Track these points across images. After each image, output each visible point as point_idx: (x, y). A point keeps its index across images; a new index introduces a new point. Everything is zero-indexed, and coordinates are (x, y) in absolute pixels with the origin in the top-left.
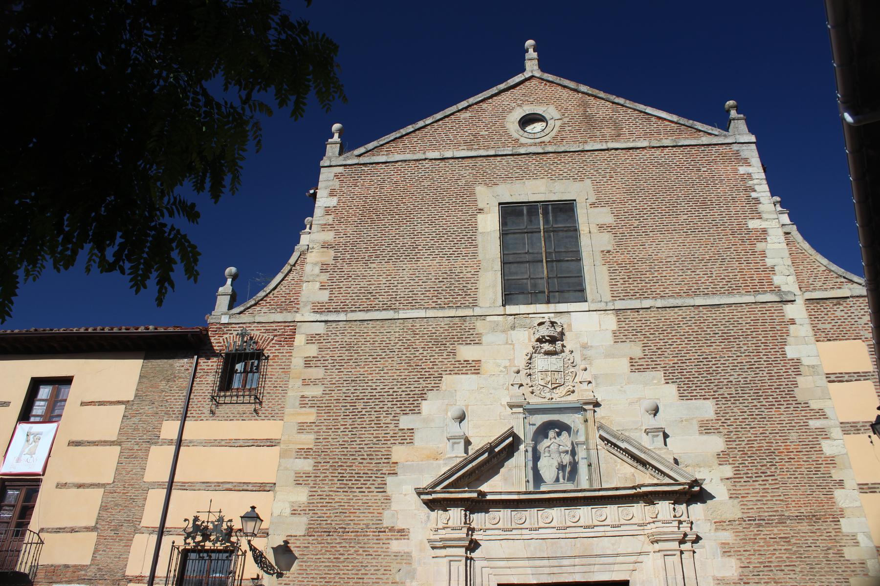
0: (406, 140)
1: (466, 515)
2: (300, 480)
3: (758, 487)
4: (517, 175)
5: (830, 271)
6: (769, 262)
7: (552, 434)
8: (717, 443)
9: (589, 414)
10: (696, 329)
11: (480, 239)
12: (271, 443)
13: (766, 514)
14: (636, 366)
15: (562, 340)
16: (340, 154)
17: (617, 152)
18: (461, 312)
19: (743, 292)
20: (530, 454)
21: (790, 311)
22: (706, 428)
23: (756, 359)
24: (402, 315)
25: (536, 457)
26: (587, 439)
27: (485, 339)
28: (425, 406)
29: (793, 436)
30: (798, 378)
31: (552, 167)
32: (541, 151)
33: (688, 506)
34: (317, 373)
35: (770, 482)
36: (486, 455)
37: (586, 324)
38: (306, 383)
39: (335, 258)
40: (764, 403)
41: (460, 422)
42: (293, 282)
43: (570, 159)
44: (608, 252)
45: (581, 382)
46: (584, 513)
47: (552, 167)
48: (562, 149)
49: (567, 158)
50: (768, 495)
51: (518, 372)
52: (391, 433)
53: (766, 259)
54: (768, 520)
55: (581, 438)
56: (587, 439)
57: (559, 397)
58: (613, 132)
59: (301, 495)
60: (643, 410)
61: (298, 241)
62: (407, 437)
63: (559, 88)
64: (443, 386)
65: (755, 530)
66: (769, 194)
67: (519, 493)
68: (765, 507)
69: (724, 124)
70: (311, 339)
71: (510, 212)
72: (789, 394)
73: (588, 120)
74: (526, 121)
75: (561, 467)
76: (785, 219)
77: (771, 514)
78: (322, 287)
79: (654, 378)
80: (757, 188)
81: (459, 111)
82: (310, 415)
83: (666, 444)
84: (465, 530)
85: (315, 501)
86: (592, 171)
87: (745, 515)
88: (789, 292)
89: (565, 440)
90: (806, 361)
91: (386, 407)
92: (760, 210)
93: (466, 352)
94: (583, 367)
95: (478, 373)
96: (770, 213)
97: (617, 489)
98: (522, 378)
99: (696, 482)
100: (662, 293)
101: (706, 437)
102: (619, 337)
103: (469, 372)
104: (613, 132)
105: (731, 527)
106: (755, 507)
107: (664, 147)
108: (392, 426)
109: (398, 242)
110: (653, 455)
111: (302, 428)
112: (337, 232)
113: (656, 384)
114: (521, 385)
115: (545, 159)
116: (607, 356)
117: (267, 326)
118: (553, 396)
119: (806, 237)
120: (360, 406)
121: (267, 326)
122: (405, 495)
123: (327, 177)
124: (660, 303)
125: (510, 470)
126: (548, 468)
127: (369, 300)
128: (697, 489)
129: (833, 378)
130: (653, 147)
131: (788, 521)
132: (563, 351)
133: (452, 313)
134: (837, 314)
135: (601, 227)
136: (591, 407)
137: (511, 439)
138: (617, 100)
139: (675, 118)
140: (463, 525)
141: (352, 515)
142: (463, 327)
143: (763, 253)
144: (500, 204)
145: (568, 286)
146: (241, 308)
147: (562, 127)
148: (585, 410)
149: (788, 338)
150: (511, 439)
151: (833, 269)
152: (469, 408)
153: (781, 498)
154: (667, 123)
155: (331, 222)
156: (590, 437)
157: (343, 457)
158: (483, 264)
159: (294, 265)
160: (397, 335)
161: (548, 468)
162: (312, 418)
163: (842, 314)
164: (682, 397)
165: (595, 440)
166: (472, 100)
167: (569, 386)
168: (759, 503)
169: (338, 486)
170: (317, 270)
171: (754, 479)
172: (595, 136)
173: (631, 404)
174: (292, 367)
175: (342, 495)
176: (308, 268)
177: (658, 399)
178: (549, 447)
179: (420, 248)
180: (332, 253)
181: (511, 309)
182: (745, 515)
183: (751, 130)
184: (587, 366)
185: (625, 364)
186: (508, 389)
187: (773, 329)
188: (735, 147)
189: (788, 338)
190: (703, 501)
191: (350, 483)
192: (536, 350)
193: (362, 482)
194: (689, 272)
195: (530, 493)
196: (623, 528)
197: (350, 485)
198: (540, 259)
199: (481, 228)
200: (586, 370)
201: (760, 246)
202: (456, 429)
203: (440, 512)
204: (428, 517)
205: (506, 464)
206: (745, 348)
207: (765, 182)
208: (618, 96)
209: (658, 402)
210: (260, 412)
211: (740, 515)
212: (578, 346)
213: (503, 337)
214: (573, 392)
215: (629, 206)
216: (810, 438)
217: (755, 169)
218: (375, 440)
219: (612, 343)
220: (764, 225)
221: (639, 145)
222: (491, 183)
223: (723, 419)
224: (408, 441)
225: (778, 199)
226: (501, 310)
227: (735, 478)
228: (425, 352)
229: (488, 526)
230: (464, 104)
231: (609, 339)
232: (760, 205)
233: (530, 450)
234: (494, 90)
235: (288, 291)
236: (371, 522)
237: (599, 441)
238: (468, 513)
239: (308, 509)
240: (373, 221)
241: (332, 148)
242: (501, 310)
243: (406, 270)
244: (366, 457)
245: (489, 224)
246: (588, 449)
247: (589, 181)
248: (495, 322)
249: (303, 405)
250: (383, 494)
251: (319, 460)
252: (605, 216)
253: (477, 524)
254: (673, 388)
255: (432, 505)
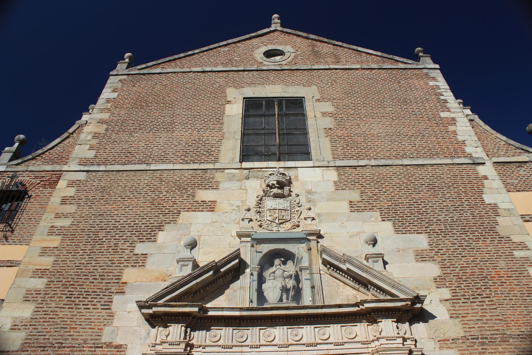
0: (178, 62)
1: (186, 332)
2: (29, 297)
3: (476, 307)
4: (259, 82)
5: (509, 144)
6: (460, 138)
7: (277, 262)
8: (433, 269)
9: (313, 244)
10: (406, 181)
11: (225, 119)
12: (11, 264)
13: (488, 333)
14: (354, 207)
15: (289, 186)
16: (127, 68)
17: (337, 71)
18: (203, 166)
19: (442, 157)
20: (255, 277)
21: (482, 170)
22: (421, 256)
23: (459, 203)
24: (153, 167)
25: (261, 280)
26: (311, 265)
27: (221, 186)
28: (161, 236)
29: (502, 264)
30: (498, 218)
31: (287, 78)
32: (279, 68)
33: (411, 325)
34: (71, 208)
35: (487, 303)
36: (211, 273)
37: (309, 177)
38: (58, 216)
39: (107, 130)
40: (471, 237)
41: (191, 250)
42: (68, 145)
43: (301, 74)
44: (330, 129)
45: (305, 219)
46: (307, 332)
47: (287, 78)
48: (295, 68)
49: (299, 73)
50: (487, 315)
51: (249, 210)
52: (126, 257)
53: (458, 137)
54: (491, 338)
55: (305, 263)
56: (311, 265)
57: (284, 230)
58: (334, 60)
59: (26, 311)
60: (362, 241)
61: (80, 118)
62: (140, 261)
63: (295, 37)
64: (180, 220)
65: (480, 348)
66: (454, 98)
67: (241, 309)
68: (486, 326)
69: (417, 58)
70: (71, 184)
71: (251, 105)
72: (492, 229)
73: (316, 54)
74: (269, 54)
75: (285, 290)
76: (468, 111)
77: (492, 332)
78: (91, 148)
79: (371, 217)
80: (443, 93)
81: (220, 47)
82: (55, 241)
83: (385, 268)
84: (183, 346)
85: (38, 317)
86: (318, 81)
87: (468, 334)
88: (479, 157)
89: (290, 268)
90: (501, 206)
91: (125, 236)
92: (448, 107)
93: (203, 195)
94: (308, 206)
95: (213, 211)
96: (456, 108)
97: (340, 306)
98: (252, 214)
99: (418, 299)
100: (375, 157)
101: (422, 264)
102: (338, 186)
103: (205, 210)
104: (334, 60)
105: (455, 345)
106: (476, 326)
107: (372, 69)
108: (127, 252)
109: (159, 120)
110: (375, 273)
111: (44, 251)
112: (113, 114)
113: (373, 221)
114: (251, 220)
115: (282, 73)
116: (330, 199)
117: (37, 174)
118: (280, 229)
119: (486, 123)
120: (101, 235)
121: (37, 174)
122: (129, 312)
123: (112, 81)
124: (373, 163)
125: (235, 291)
126: (272, 291)
127: (128, 157)
128: (418, 306)
129: (527, 218)
130: (364, 69)
131: (511, 340)
132: (290, 195)
133: (196, 166)
134: (521, 173)
135: (324, 114)
136: (315, 238)
137: (237, 261)
138: (337, 43)
139: (379, 54)
140: (182, 340)
141: (72, 330)
142: (204, 177)
143: (455, 133)
144: (244, 98)
145: (296, 147)
146: (19, 161)
147: (296, 57)
148: (309, 240)
149: (484, 189)
150: (237, 261)
151: (511, 143)
152: (202, 238)
153: (500, 317)
154: (373, 57)
155: (109, 107)
156: (314, 263)
157: (75, 277)
158: (227, 135)
159: (72, 134)
160: (146, 182)
161: (272, 291)
162: (56, 244)
163: (525, 173)
164: (397, 231)
165: (318, 264)
166: (230, 41)
167: (295, 221)
168: (479, 322)
169: (65, 302)
170: (90, 137)
171: (472, 300)
172: (321, 62)
173: (351, 236)
174: (50, 204)
175: (67, 312)
176: (82, 136)
177: (376, 233)
178: (274, 273)
179: (176, 124)
180: (105, 126)
181: (245, 165)
182: (468, 334)
183: (435, 62)
184: (311, 207)
185: (345, 206)
186: (238, 223)
187: (470, 182)
188: (425, 71)
189: (484, 189)
190: (426, 321)
191: (77, 300)
192: (266, 194)
193: (90, 299)
194: (397, 143)
195: (252, 309)
196: (346, 346)
197: (77, 302)
198: (273, 131)
199: (227, 112)
200: (310, 209)
201: (451, 128)
202: (187, 253)
203: (161, 329)
204: (148, 334)
205: (231, 286)
206: (449, 195)
207: (449, 91)
208: (337, 41)
209: (376, 235)
210: (10, 238)
211: (462, 334)
212: (304, 191)
213: (237, 184)
214: (298, 226)
215: (346, 102)
216: (517, 265)
217: (442, 83)
218: (109, 263)
219: (334, 190)
220: (453, 115)
221: (353, 67)
222: (238, 85)
223: (436, 250)
224: (141, 264)
225: (461, 101)
226: (238, 165)
227: (454, 300)
228: (168, 195)
229: (208, 343)
230: (225, 43)
231: (331, 187)
232: (448, 104)
233: (255, 273)
234: (248, 36)
235: (62, 150)
236: (90, 338)
237: (322, 267)
238: (189, 330)
239: (32, 323)
240: (142, 107)
241: (121, 67)
242: (238, 165)
243: (162, 138)
244: (98, 277)
245: (235, 110)
246: (311, 273)
247: (315, 87)
248: (232, 173)
249: (50, 233)
250: (107, 311)
251: (53, 279)
252: (328, 107)
253: (198, 341)
254: (389, 225)
255: (155, 320)
